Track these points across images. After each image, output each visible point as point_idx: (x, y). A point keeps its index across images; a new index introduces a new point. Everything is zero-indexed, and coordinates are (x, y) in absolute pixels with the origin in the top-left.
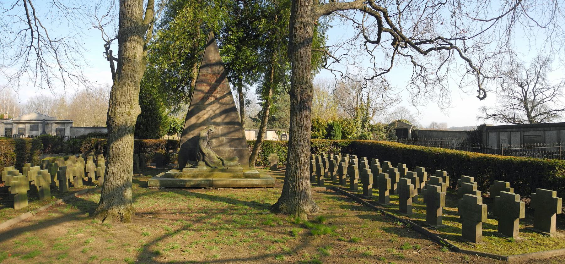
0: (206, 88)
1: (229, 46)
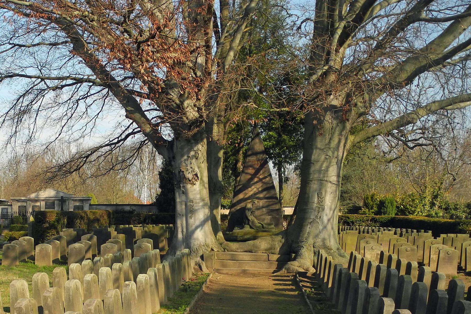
0: (251, 171)
1: (271, 133)
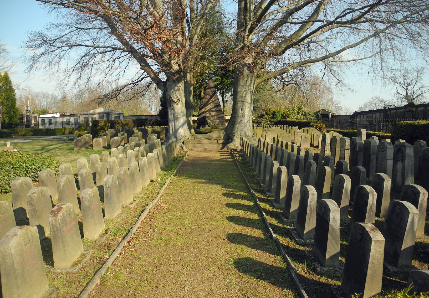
0: (208, 97)
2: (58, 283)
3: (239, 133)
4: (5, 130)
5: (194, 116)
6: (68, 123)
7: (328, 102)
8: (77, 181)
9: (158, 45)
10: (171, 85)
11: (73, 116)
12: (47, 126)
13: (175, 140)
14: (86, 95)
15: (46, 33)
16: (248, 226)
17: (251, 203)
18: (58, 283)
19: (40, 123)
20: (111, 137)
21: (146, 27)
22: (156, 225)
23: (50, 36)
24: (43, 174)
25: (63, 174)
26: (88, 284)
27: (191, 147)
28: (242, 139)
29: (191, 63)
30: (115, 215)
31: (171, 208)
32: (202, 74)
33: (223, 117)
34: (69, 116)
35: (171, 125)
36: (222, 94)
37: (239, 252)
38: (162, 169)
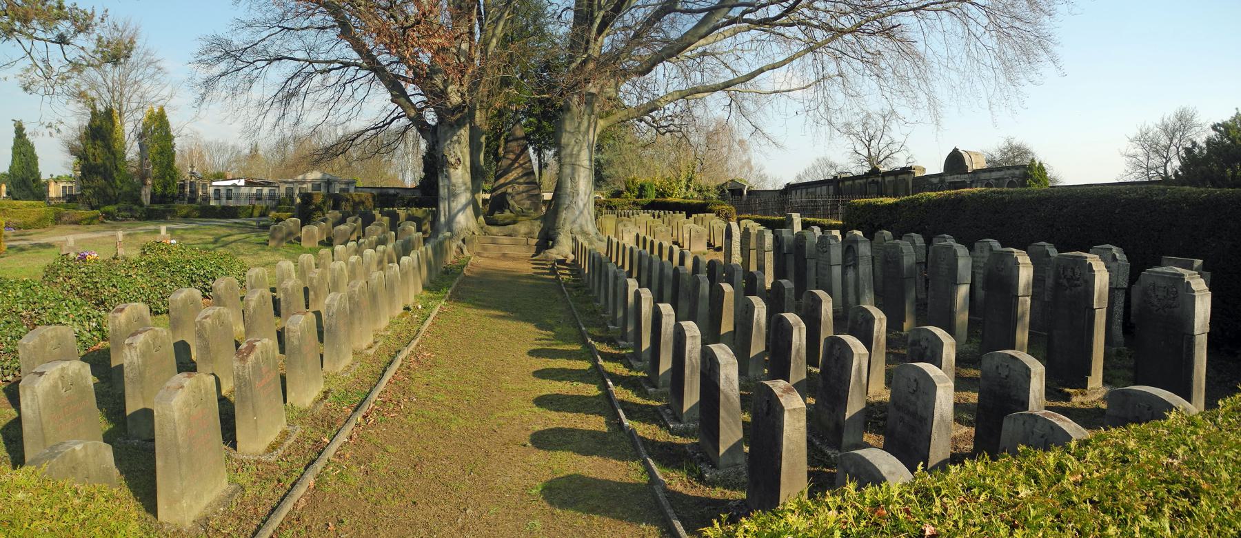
0: (512, 156)
2: (243, 478)
3: (568, 227)
4: (156, 207)
5: (485, 191)
6: (259, 197)
7: (742, 167)
8: (276, 302)
9: (425, 58)
10: (445, 133)
11: (268, 184)
12: (224, 202)
13: (448, 234)
14: (291, 147)
15: (230, 37)
16: (577, 411)
17: (585, 365)
18: (243, 478)
19: (212, 195)
20: (334, 225)
21: (406, 24)
22: (414, 389)
23: (236, 42)
24: (221, 284)
25: (252, 288)
26: (293, 485)
27: (477, 249)
28: (574, 240)
29: (483, 90)
30: (341, 367)
31: (441, 359)
32: (500, 113)
33: (538, 196)
34: (260, 184)
35: (443, 206)
36: (539, 152)
37: (555, 467)
38: (424, 288)
